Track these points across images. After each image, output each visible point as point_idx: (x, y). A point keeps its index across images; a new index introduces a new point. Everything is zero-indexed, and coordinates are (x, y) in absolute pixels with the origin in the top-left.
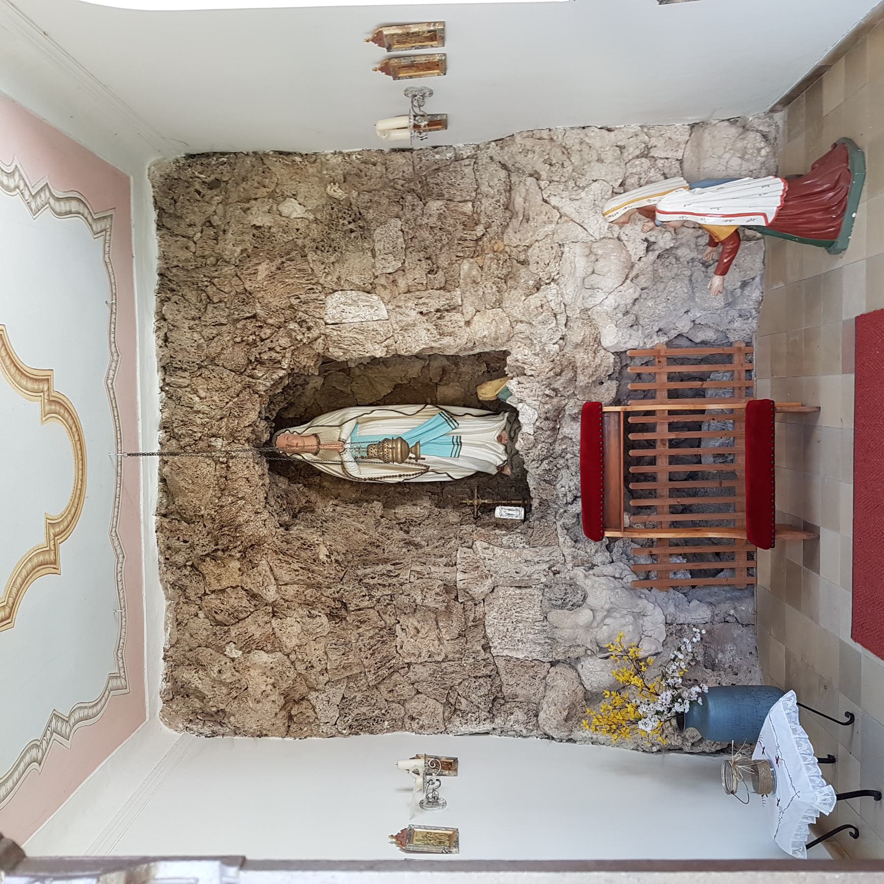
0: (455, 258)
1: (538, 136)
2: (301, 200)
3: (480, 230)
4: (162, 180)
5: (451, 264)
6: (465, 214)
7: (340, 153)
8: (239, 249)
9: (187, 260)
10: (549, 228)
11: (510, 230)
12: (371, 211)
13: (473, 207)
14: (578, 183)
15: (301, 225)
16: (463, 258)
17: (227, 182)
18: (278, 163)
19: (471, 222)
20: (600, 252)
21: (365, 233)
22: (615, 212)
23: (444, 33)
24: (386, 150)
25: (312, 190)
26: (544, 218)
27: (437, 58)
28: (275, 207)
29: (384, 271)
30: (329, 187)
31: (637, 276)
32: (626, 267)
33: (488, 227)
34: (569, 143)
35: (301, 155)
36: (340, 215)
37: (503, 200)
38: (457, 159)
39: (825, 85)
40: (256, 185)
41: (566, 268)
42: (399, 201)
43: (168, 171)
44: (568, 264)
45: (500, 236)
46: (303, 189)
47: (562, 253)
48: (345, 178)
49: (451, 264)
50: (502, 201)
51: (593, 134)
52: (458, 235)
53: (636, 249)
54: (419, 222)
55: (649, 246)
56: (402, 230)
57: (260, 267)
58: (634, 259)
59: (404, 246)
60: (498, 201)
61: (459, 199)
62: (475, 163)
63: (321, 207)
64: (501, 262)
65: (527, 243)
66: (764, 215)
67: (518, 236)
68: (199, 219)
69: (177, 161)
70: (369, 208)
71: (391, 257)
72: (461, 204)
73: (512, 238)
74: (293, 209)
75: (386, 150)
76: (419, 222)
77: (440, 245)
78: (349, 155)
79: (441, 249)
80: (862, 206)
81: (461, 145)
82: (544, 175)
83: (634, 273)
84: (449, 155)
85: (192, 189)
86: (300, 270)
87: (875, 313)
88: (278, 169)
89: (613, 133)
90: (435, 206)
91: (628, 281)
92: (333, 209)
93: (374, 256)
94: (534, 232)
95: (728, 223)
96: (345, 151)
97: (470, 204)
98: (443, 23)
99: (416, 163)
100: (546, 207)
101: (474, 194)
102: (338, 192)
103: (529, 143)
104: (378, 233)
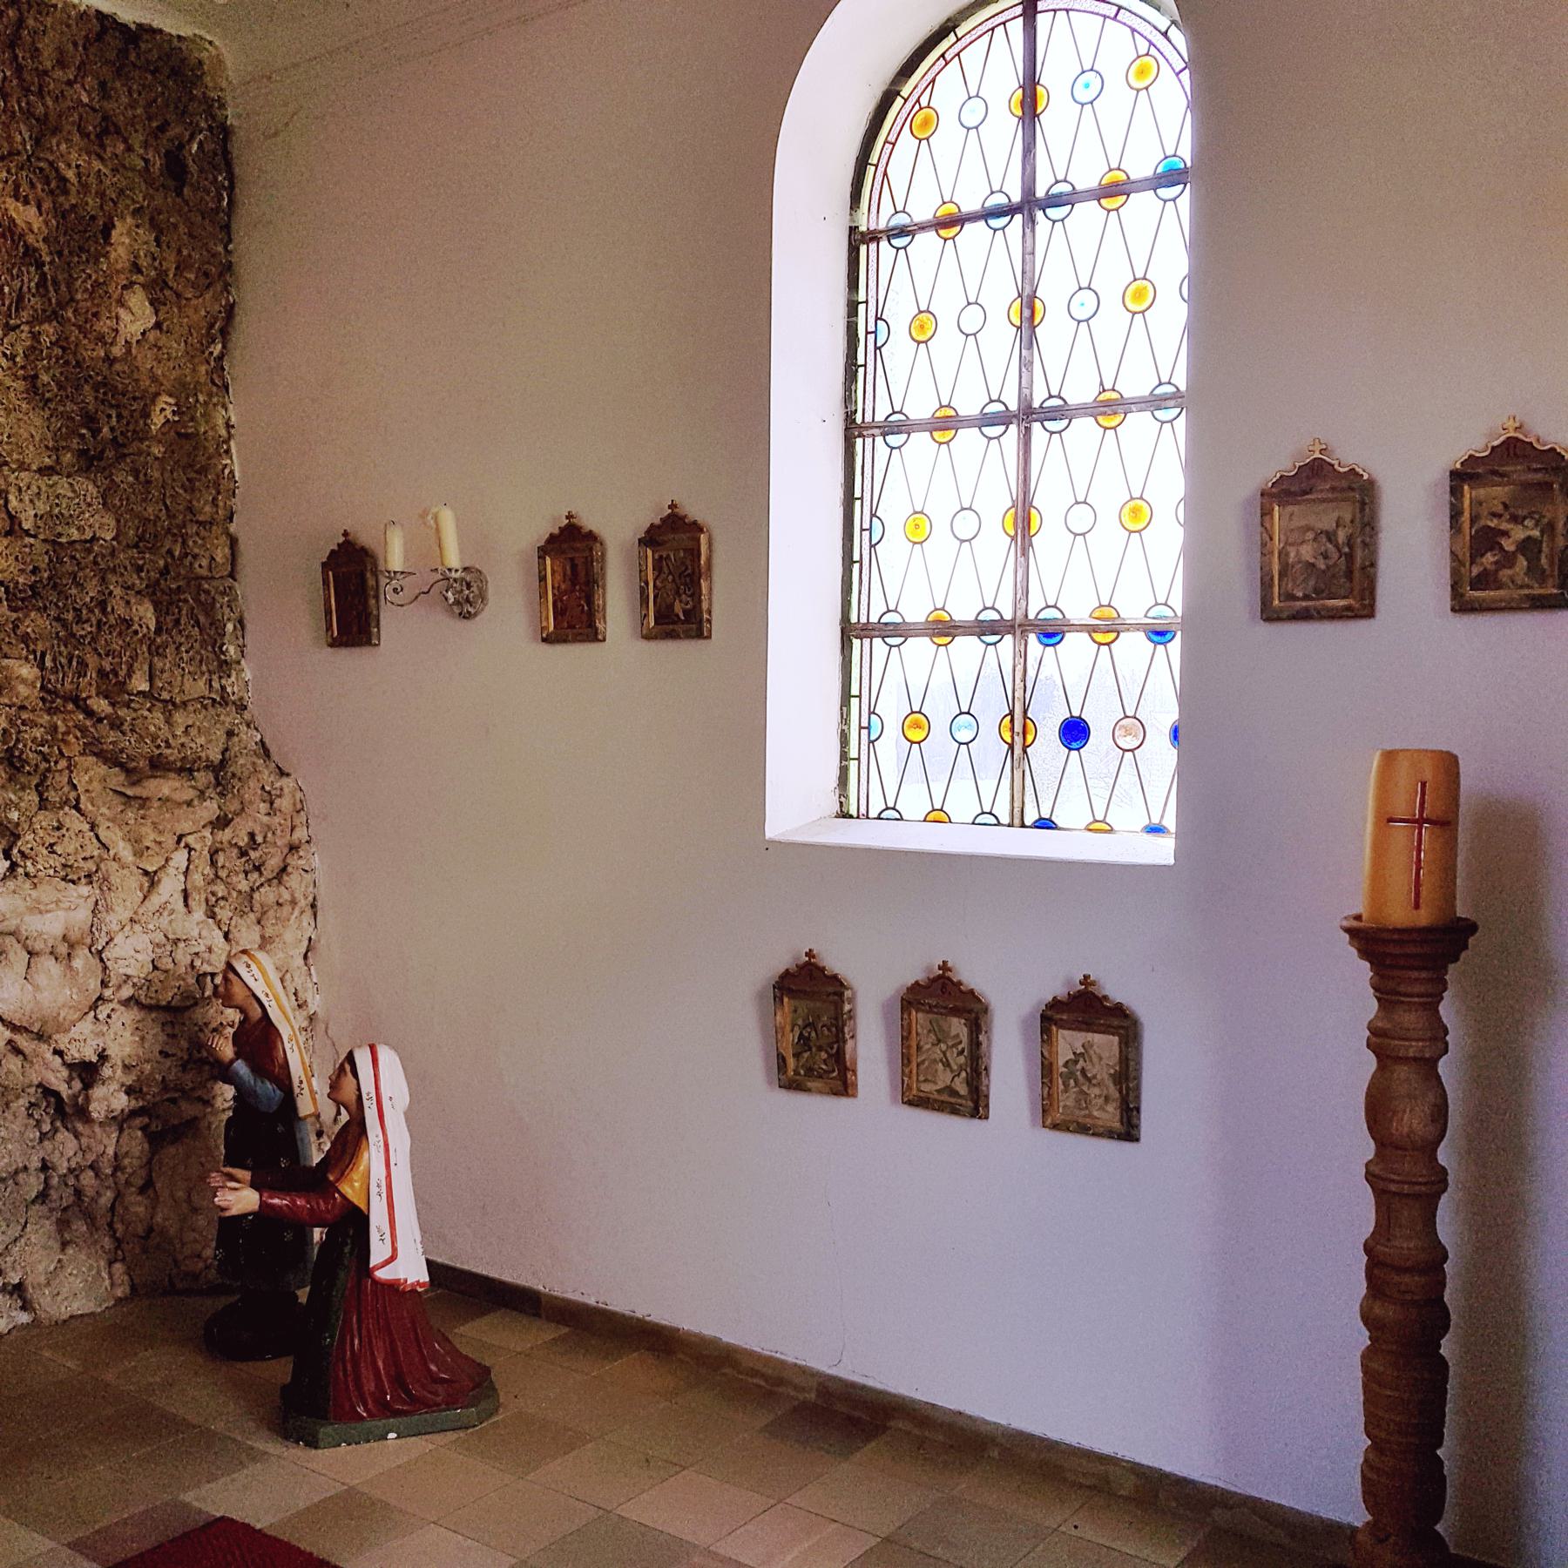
0: (40, 647)
1: (297, 821)
2: (151, 336)
3: (101, 705)
4: (194, 61)
5: (25, 639)
6: (129, 675)
7: (230, 436)
8: (70, 174)
9: (35, 53)
10: (125, 851)
11: (103, 769)
12: (131, 479)
13: (140, 692)
14: (222, 903)
15: (103, 325)
16: (42, 666)
17: (179, 193)
18: (217, 308)
19: (113, 686)
20: (78, 963)
21: (89, 462)
22: (258, 975)
23: (689, 636)
24: (233, 528)
25: (171, 364)
26: (150, 837)
27: (600, 626)
28: (141, 279)
29: (13, 489)
30: (172, 401)
31: (17, 1051)
32: (44, 1023)
33: (116, 724)
34: (293, 880)
35: (221, 358)
36: (125, 413)
37: (172, 754)
38: (225, 667)
39: (487, 1319)
40: (185, 252)
41: (46, 892)
42: (145, 541)
43: (208, 79)
44: (55, 895)
45: (96, 749)
46: (176, 348)
47: (73, 882)
48: (187, 436)
49: (25, 639)
50: (169, 751)
51: (305, 924)
52: (92, 660)
53: (83, 1042)
54: (112, 578)
55: (87, 1072)
56: (94, 539)
57: (33, 210)
58: (62, 1041)
59: (63, 540)
60: (168, 746)
61: (159, 664)
62: (214, 700)
63: (136, 376)
64: (45, 749)
65: (85, 804)
66: (393, 1258)
67: (96, 786)
68: (118, 106)
69: (222, 106)
70: (137, 478)
71: (42, 507)
72: (146, 667)
73: (92, 775)
74: (135, 317)
75: (233, 528)
76: (112, 578)
77: (70, 616)
78: (228, 451)
79: (58, 619)
80: (419, 1445)
81: (248, 675)
82: (225, 835)
83: (22, 1041)
84: (232, 650)
85: (171, 117)
86: (20, 298)
87: (288, 1546)
88: (202, 307)
89: (302, 962)
90: (146, 614)
91: (8, 1034)
92: (135, 399)
93: (44, 471)
94: (113, 820)
95: (374, 1190)
96: (232, 443)
97: (145, 687)
98: (709, 637)
99: (215, 583)
100: (170, 841)
101: (165, 696)
102: (162, 412)
103: (284, 804)
104: (89, 488)
